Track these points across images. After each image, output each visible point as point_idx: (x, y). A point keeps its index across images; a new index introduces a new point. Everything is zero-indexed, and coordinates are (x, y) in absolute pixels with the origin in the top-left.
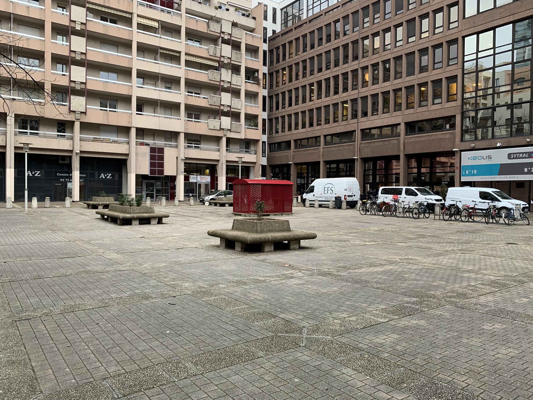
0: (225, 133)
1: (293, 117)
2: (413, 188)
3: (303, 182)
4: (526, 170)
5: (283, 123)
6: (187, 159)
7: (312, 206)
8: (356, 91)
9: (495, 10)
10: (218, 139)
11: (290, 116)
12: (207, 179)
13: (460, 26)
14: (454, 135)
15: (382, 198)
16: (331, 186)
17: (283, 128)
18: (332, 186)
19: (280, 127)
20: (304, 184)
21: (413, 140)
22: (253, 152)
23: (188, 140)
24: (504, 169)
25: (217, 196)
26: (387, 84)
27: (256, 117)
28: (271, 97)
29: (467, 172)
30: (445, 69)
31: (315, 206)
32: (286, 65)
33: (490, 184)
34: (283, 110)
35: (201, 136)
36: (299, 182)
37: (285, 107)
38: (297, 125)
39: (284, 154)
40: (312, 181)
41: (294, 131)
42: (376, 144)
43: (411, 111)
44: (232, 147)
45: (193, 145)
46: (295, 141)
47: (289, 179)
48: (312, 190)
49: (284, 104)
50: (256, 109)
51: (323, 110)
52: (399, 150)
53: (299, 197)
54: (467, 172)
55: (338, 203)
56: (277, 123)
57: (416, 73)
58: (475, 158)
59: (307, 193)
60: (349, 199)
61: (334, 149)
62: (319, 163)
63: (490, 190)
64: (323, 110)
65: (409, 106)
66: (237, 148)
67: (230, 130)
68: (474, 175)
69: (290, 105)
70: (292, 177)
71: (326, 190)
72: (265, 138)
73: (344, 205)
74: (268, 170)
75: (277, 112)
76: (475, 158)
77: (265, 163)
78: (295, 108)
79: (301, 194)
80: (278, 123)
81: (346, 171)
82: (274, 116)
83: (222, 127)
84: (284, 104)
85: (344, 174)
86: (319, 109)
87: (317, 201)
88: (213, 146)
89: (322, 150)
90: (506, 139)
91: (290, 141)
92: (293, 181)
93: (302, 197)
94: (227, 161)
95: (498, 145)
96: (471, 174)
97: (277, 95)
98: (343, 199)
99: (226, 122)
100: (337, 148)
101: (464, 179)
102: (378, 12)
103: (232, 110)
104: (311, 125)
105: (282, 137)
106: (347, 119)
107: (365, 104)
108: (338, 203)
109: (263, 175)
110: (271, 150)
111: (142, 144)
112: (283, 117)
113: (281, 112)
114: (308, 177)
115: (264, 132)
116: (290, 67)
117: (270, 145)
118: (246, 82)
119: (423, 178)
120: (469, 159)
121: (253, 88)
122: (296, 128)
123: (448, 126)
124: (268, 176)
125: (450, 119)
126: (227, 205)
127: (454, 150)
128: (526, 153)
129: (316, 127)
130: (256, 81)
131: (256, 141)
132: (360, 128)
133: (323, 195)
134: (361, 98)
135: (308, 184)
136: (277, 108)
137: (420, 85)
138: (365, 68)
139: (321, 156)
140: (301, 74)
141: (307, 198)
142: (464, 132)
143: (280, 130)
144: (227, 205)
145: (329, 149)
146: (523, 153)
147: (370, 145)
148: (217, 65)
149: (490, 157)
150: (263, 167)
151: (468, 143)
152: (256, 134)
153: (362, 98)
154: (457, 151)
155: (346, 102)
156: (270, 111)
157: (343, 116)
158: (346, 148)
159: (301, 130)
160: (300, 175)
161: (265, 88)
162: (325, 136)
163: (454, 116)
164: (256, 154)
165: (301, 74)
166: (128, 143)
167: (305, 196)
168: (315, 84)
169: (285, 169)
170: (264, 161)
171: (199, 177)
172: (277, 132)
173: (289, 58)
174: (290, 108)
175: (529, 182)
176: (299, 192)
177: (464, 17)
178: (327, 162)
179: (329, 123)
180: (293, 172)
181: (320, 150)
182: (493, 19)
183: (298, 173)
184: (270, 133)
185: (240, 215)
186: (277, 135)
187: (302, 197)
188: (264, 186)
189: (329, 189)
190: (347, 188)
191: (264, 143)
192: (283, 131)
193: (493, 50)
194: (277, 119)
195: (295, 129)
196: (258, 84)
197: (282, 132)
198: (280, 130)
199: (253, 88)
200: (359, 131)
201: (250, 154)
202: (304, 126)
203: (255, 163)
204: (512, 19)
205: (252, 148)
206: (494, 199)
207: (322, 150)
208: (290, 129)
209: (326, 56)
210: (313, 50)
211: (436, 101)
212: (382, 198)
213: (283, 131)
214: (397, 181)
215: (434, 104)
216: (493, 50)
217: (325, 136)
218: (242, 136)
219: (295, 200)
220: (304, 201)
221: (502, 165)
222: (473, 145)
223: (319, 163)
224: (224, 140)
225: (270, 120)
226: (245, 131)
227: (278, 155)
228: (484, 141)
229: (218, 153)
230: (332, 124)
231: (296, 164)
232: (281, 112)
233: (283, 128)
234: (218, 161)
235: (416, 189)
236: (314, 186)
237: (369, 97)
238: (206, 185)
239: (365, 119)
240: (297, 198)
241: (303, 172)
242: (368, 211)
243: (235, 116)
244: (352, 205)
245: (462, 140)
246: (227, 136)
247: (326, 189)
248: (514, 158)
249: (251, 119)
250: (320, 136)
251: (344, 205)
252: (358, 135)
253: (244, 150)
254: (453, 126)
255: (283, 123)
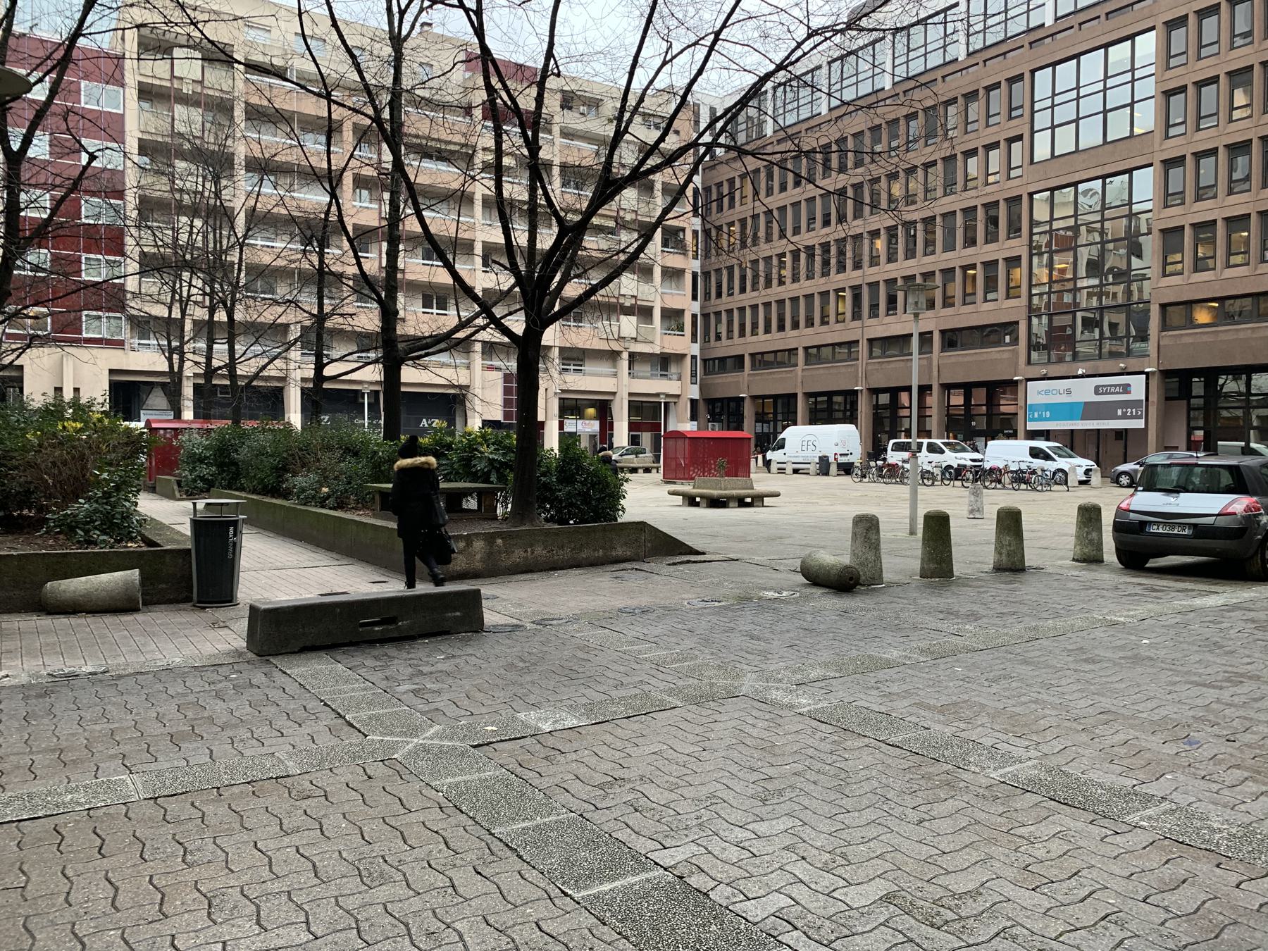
0: (627, 345)
1: (748, 312)
2: (938, 442)
3: (766, 430)
4: (1120, 412)
5: (730, 323)
6: (563, 391)
7: (782, 471)
8: (859, 273)
9: (1076, 155)
10: (613, 356)
11: (742, 310)
12: (594, 426)
13: (1025, 177)
14: (1016, 353)
15: (894, 457)
16: (814, 438)
17: (730, 331)
18: (814, 438)
19: (723, 329)
20: (768, 435)
21: (953, 360)
22: (675, 377)
23: (563, 359)
24: (1091, 410)
25: (621, 455)
26: (911, 262)
27: (679, 313)
28: (706, 275)
29: (1036, 415)
30: (1003, 243)
31: (787, 472)
32: (735, 218)
33: (1046, 435)
34: (730, 299)
35: (584, 351)
36: (759, 430)
37: (732, 294)
38: (755, 326)
39: (730, 380)
40: (784, 428)
41: (749, 338)
42: (892, 365)
43: (949, 311)
44: (637, 367)
45: (572, 367)
46: (752, 355)
47: (739, 427)
48: (781, 446)
49: (730, 288)
50: (682, 299)
51: (802, 302)
52: (930, 377)
53: (760, 457)
54: (1036, 415)
55: (824, 467)
56: (719, 321)
57: (957, 248)
58: (1047, 392)
59: (773, 450)
60: (842, 460)
61: (821, 372)
62: (795, 395)
63: (1042, 444)
64: (802, 302)
65: (948, 302)
66: (645, 369)
67: (635, 339)
68: (1046, 419)
69: (743, 290)
70: (746, 421)
71: (804, 445)
72: (695, 349)
73: (833, 469)
74: (702, 408)
75: (719, 301)
76: (1047, 392)
77: (696, 396)
78: (749, 298)
79: (764, 452)
80: (721, 322)
81: (845, 411)
82: (712, 310)
83: (622, 335)
84: (730, 288)
85: (840, 415)
86: (795, 300)
87: (789, 464)
88: (605, 368)
89: (800, 373)
90: (1092, 363)
91: (743, 356)
92: (750, 428)
93: (764, 457)
94: (630, 394)
95: (1080, 372)
96: (1040, 419)
97: (718, 271)
98: (832, 460)
99: (628, 325)
100: (827, 372)
101: (1032, 426)
102: (897, 137)
103: (639, 303)
104: (781, 328)
105: (727, 348)
106: (844, 321)
107: (930, 231)
108: (824, 467)
109: (694, 417)
110: (707, 371)
111: (491, 368)
112: (730, 312)
113: (725, 303)
114: (775, 420)
115: (694, 340)
116: (743, 222)
117: (705, 361)
118: (663, 251)
119: (974, 424)
120: (1039, 393)
121: (675, 261)
122: (754, 332)
123: (1008, 339)
124: (701, 419)
125: (1010, 327)
126: (641, 471)
127: (1016, 378)
128: (1119, 385)
129: (789, 332)
130: (681, 247)
131: (682, 357)
132: (866, 337)
133: (800, 454)
134: (869, 284)
135: (776, 434)
136: (719, 295)
137: (965, 268)
138: (875, 234)
139: (800, 384)
140: (762, 234)
141: (773, 459)
142: (1032, 346)
143: (724, 335)
144: (641, 471)
145: (814, 372)
146: (1115, 386)
147: (883, 366)
148: (612, 224)
149: (1069, 392)
150: (693, 402)
151: (1037, 367)
152: (684, 344)
153: (869, 284)
154: (1021, 381)
155: (843, 290)
156: (705, 300)
157: (838, 314)
158: (843, 370)
159: (762, 337)
160: (760, 418)
161: (695, 257)
162: (806, 349)
163: (1017, 323)
164: (679, 379)
165: (762, 234)
166: (468, 367)
167: (770, 455)
168: (788, 255)
169: (732, 405)
170: (694, 392)
171: (580, 422)
172: (718, 338)
173: (741, 205)
174: (743, 296)
175: (1096, 433)
176: (759, 448)
177: (1032, 162)
178: (808, 395)
179: (812, 325)
180: (748, 411)
181: (797, 375)
182: (1073, 170)
183: (757, 414)
184: (706, 339)
185: (675, 483)
186: (718, 344)
187: (764, 457)
188: (694, 440)
189: (810, 443)
190: (839, 442)
191: (694, 357)
192: (729, 337)
193: (1073, 219)
194: (718, 314)
195: (752, 335)
196: (685, 254)
197: (728, 338)
198: (724, 335)
199: (675, 261)
200: (865, 341)
201: (670, 379)
202: (768, 330)
203: (678, 396)
204: (1099, 172)
205: (673, 369)
206: (1047, 457)
207: (800, 373)
208: (742, 333)
209: (808, 206)
210: (783, 194)
211: (990, 296)
212: (894, 457)
213: (729, 337)
214: (908, 433)
215: (986, 300)
216: (1073, 219)
217: (806, 349)
218: (657, 350)
219: (753, 462)
220: (767, 463)
221: (1086, 403)
222: (1044, 371)
223: (795, 395)
224: (625, 355)
225: (706, 316)
226: (662, 339)
227: (720, 381)
228: (1062, 364)
229: (614, 380)
230: (818, 327)
231: (754, 398)
232: (725, 303)
233: (730, 331)
234: (614, 394)
235: (943, 443)
236: (784, 439)
237: (882, 284)
238: (592, 437)
239: (874, 321)
240: (757, 458)
241: (766, 411)
242: (865, 477)
243: (645, 313)
244: (846, 469)
245: (1029, 362)
246: (631, 350)
247: (805, 443)
248: (1102, 394)
249: (672, 316)
250: (797, 349)
251: (833, 469)
252: (863, 348)
253: (659, 372)
254: (1015, 341)
255: (730, 323)
